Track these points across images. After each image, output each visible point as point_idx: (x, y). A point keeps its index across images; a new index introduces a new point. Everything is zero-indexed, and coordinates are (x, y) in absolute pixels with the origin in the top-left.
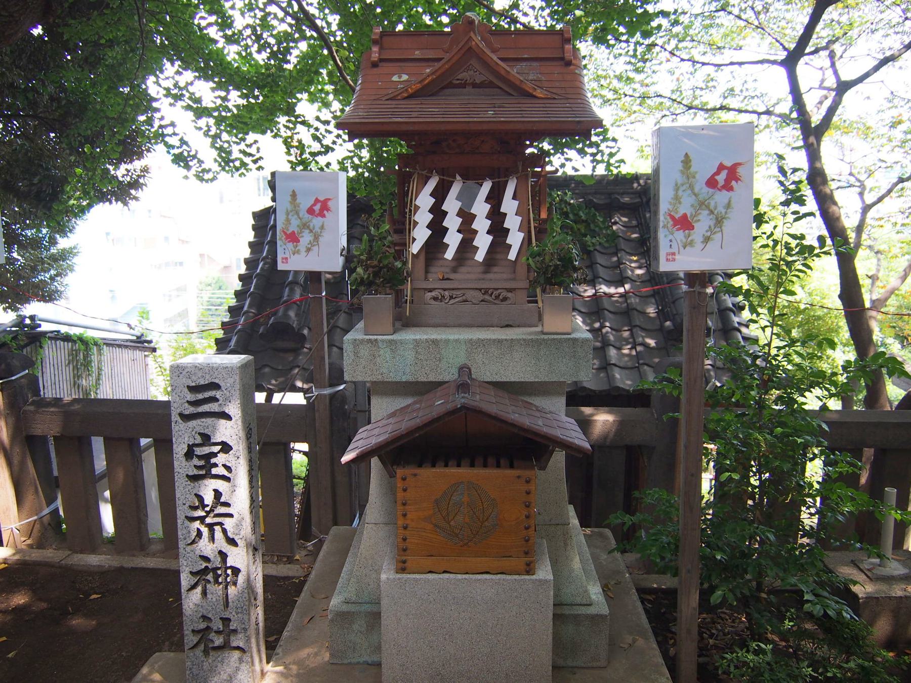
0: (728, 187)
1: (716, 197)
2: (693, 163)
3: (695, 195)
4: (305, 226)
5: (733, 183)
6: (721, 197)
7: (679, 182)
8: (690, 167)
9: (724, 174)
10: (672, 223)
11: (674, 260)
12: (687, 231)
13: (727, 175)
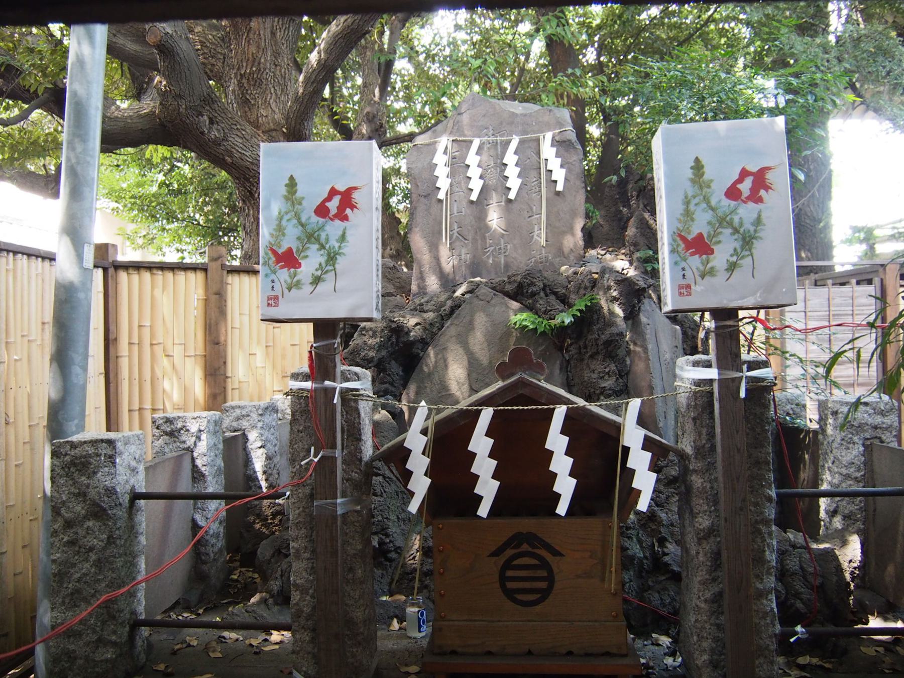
1: (327, 228)
2: (299, 187)
4: (723, 221)
5: (348, 211)
6: (334, 228)
7: (690, 194)
8: (296, 191)
9: (336, 200)
10: (683, 246)
11: (277, 305)
12: (704, 257)
13: (753, 182)
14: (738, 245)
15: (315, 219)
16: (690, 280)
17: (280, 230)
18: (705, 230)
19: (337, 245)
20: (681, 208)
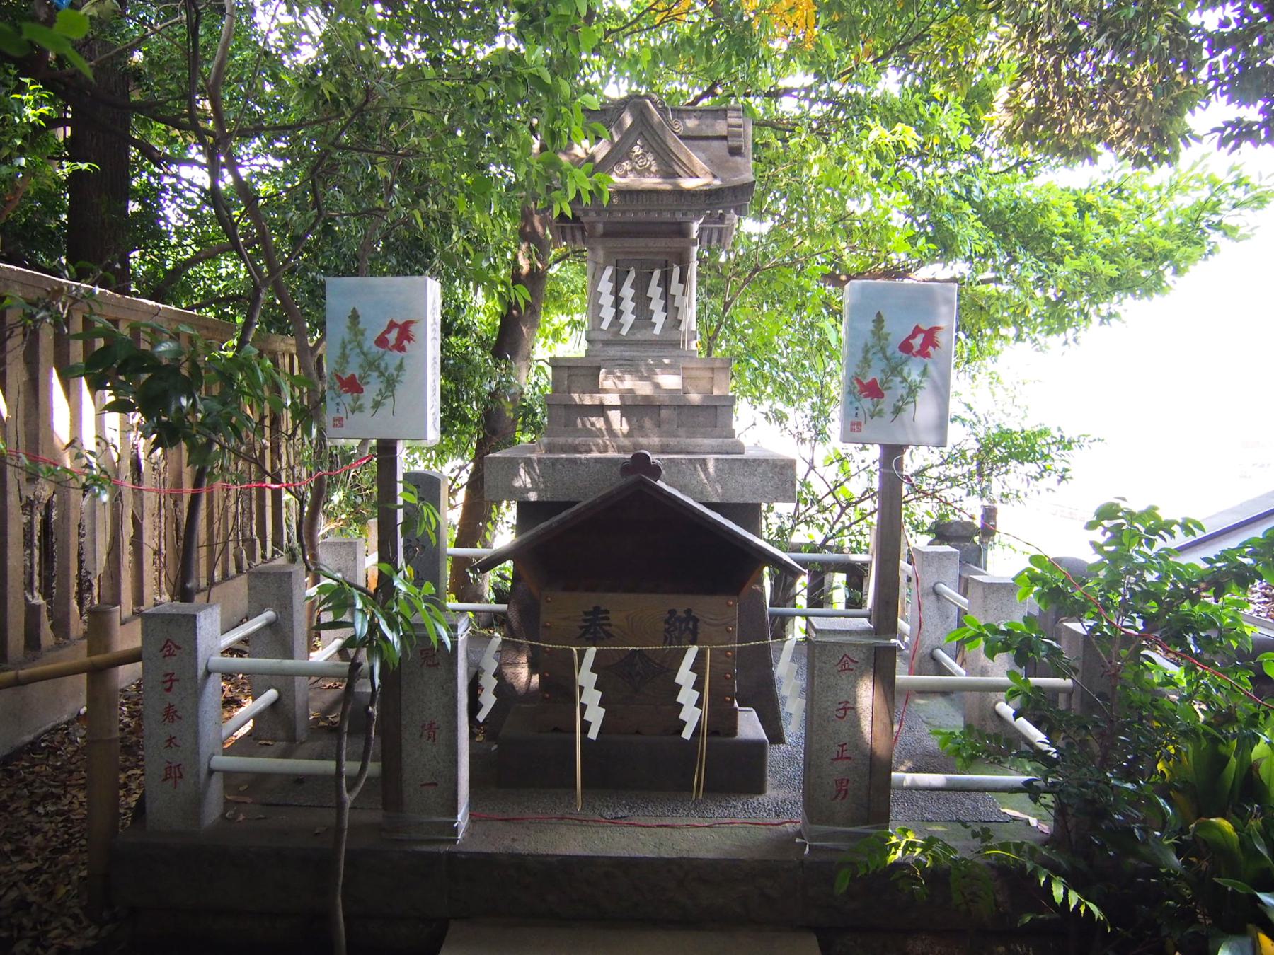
0: (924, 353)
3: (887, 359)
6: (392, 358)
11: (342, 426)
14: (383, 386)
15: (375, 349)
16: (343, 414)
17: (344, 357)
18: (357, 373)
19: (918, 379)
20: (860, 356)
